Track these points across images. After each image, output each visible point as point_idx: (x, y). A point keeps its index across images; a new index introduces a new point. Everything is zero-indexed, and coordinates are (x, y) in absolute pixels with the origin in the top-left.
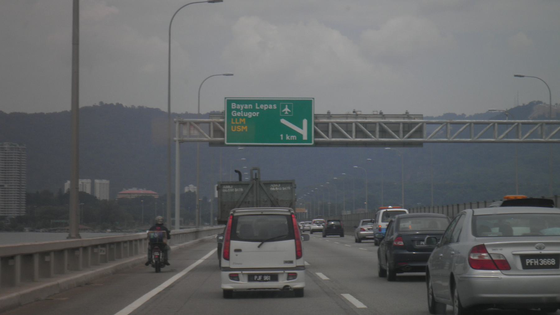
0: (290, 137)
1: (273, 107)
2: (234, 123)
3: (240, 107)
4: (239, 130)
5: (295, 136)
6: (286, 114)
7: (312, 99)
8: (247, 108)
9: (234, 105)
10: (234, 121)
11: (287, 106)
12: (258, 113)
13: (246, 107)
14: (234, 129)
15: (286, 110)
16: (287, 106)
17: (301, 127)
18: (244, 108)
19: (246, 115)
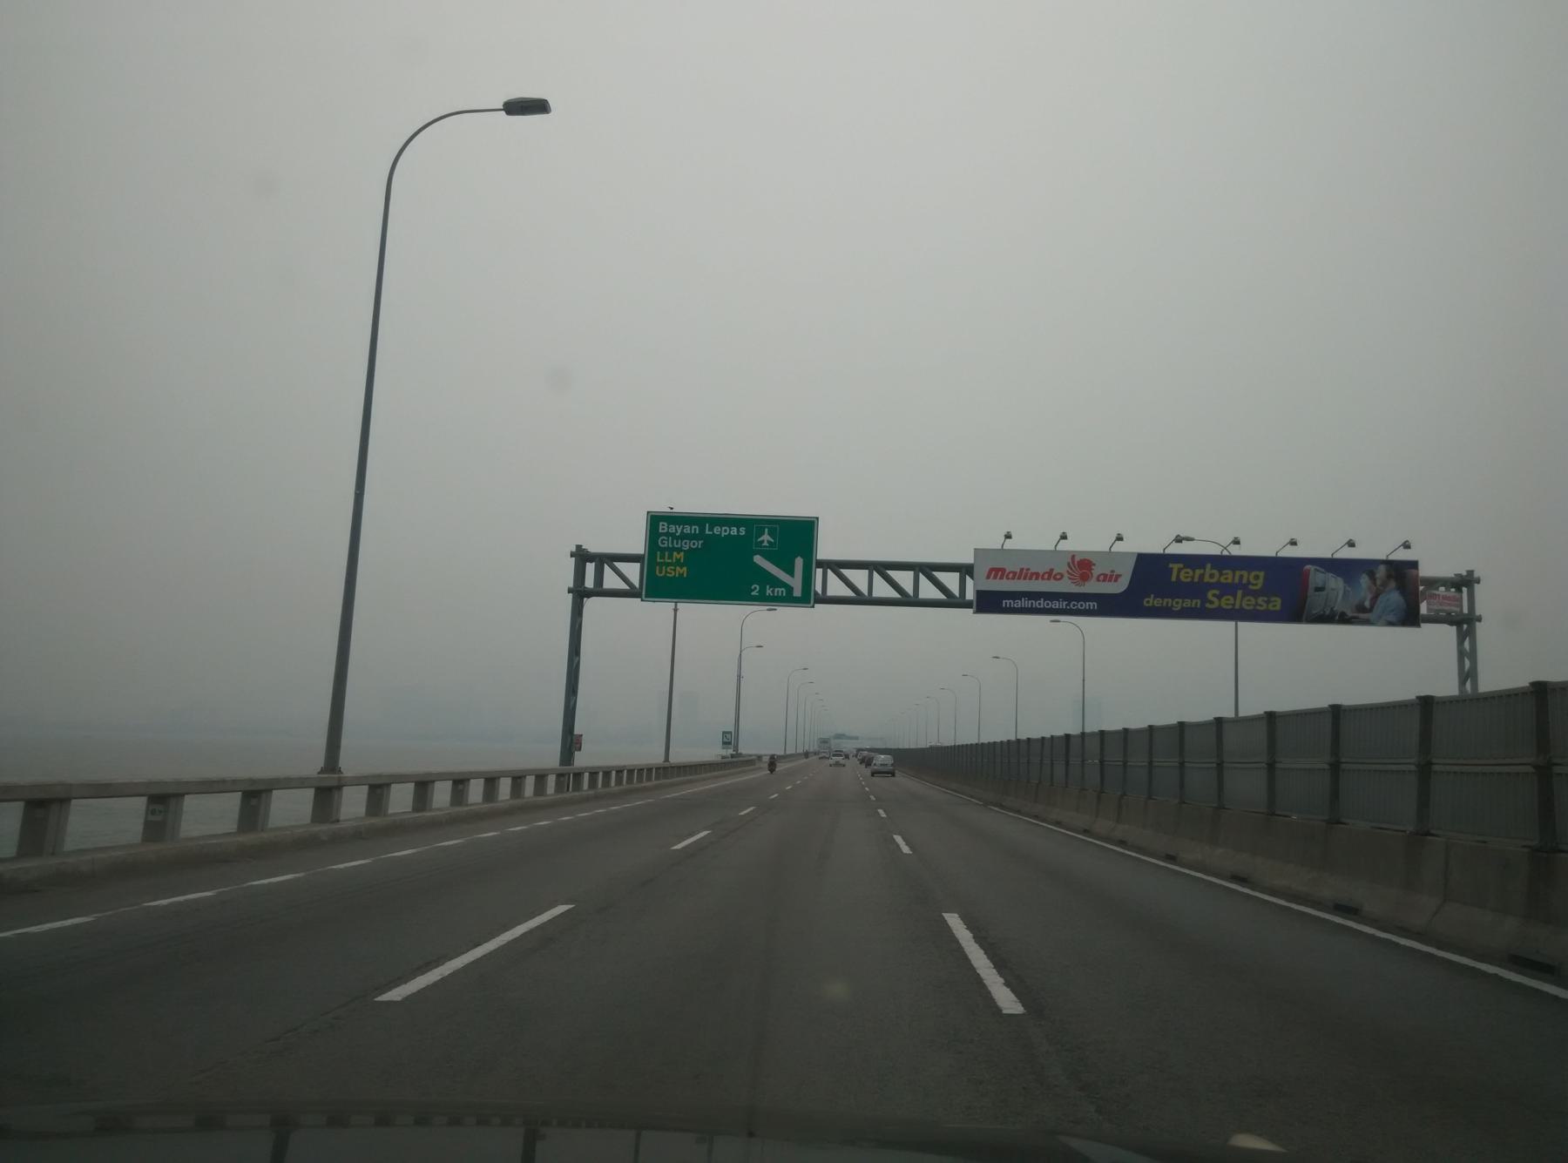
0: (773, 592)
1: (738, 531)
2: (662, 561)
3: (676, 530)
4: (671, 573)
5: (783, 589)
6: (765, 546)
7: (650, 514)
8: (1230, 581)
9: (663, 525)
10: (662, 557)
11: (766, 530)
12: (700, 542)
13: (687, 530)
14: (660, 573)
15: (766, 537)
16: (766, 530)
17: (791, 573)
18: (682, 532)
19: (679, 546)
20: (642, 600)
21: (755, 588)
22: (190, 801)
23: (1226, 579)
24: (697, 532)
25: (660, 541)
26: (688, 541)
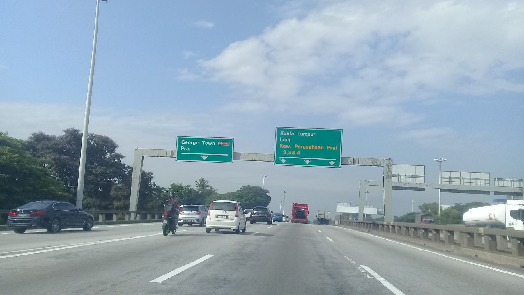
7: (341, 131)
21: (285, 152)
22: (219, 229)
24: (290, 141)
25: (182, 141)
26: (195, 142)
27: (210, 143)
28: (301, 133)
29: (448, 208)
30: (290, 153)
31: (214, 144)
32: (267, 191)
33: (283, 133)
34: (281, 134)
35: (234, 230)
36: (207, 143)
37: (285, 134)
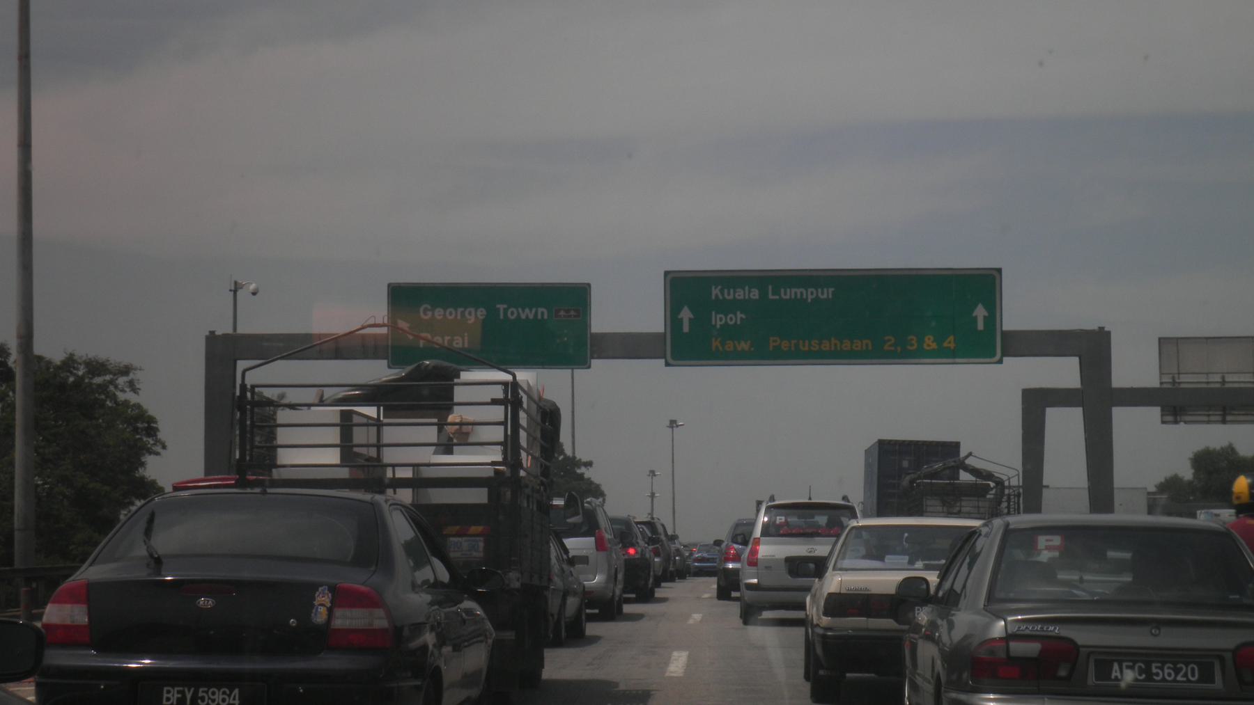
12: (831, 290)
20: (667, 364)
23: (729, 347)
24: (546, 317)
27: (527, 310)
28: (782, 290)
29: (468, 699)
30: (912, 345)
31: (543, 313)
32: (1190, 459)
33: (723, 294)
34: (713, 297)
35: (1206, 676)
36: (512, 313)
37: (729, 294)
